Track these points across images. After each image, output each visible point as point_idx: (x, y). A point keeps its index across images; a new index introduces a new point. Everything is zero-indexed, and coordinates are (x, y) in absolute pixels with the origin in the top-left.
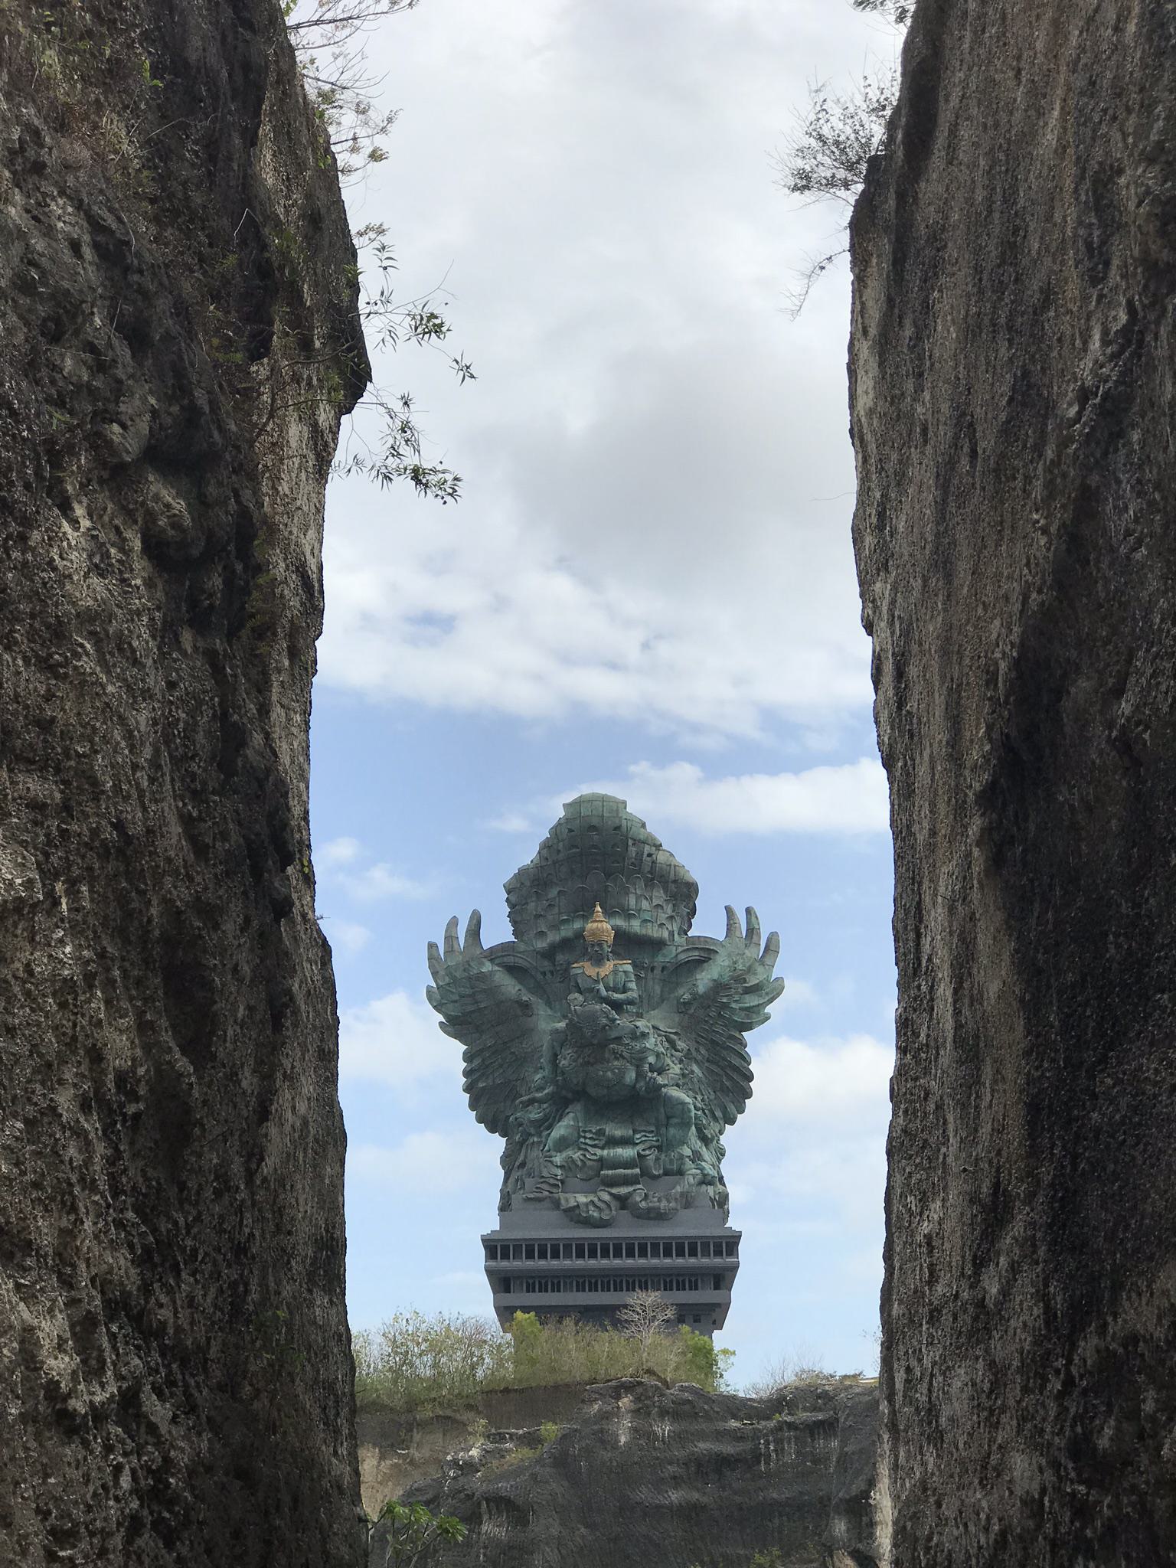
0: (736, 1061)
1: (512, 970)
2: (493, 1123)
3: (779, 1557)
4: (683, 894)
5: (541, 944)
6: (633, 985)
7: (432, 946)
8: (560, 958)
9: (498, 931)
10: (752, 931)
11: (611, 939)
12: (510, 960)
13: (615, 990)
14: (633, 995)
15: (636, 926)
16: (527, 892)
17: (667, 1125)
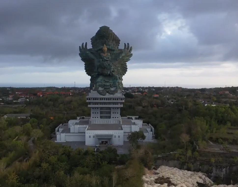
0: (125, 67)
1: (92, 53)
2: (89, 74)
3: (129, 134)
4: (117, 41)
5: (96, 50)
6: (110, 57)
7: (80, 47)
8: (99, 52)
9: (90, 46)
10: (128, 47)
11: (107, 50)
12: (91, 51)
13: (107, 58)
14: (110, 59)
15: (110, 47)
16: (94, 40)
17: (115, 79)
